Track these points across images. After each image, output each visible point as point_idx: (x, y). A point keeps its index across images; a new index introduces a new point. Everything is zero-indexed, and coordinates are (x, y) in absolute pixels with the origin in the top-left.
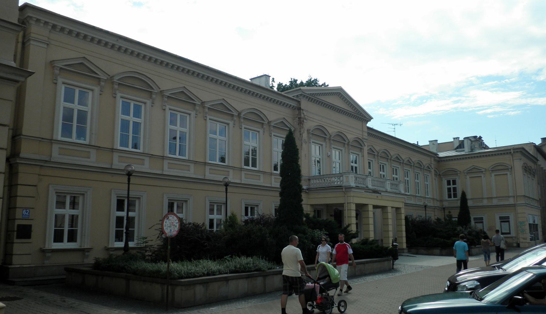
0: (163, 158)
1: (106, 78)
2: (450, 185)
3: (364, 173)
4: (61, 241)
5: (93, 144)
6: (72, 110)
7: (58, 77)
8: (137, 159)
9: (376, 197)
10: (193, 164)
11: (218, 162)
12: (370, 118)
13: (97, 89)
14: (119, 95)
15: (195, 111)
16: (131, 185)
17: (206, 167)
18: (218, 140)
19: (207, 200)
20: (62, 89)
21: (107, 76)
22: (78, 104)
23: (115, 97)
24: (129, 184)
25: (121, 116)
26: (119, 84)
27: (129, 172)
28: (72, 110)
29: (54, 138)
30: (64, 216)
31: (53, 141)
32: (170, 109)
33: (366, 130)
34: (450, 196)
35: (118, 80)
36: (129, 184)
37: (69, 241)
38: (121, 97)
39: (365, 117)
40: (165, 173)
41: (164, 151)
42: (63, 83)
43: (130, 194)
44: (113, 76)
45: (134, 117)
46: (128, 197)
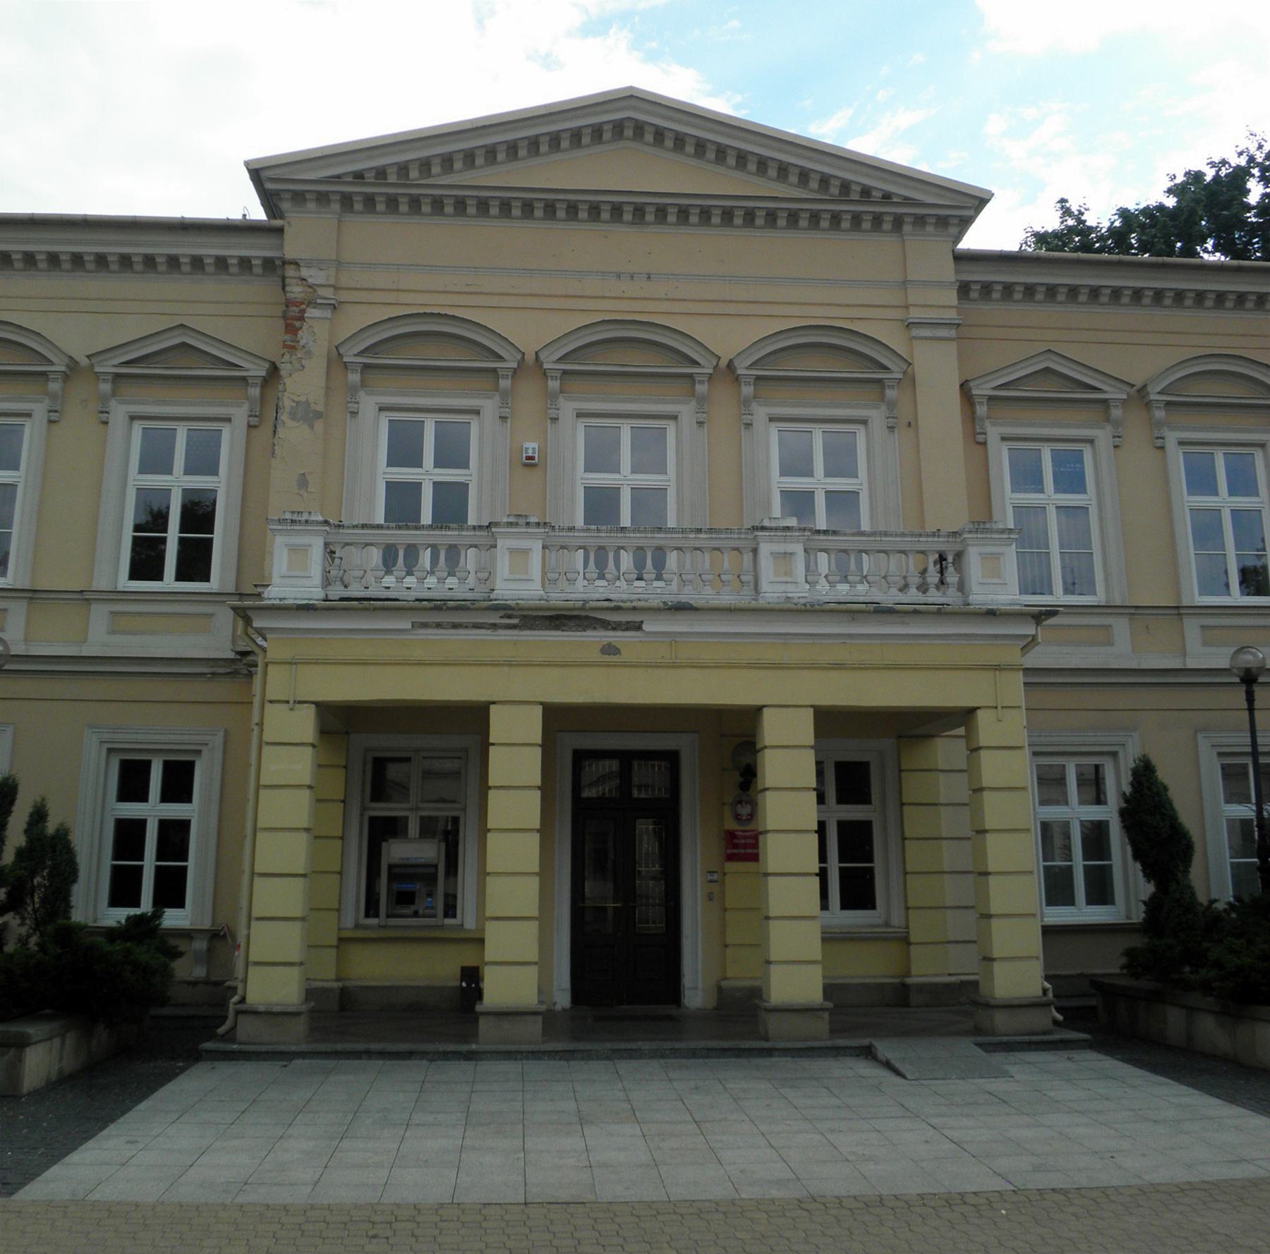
0: (1178, 611)
1: (1125, 397)
2: (415, 460)
3: (923, 527)
4: (1069, 901)
5: (1118, 603)
6: (416, 487)
7: (987, 424)
8: (1259, 627)
9: (596, 656)
10: (24, 604)
11: (1237, 597)
12: (970, 203)
13: (1103, 436)
14: (1172, 438)
15: (1109, 428)
16: (1257, 714)
17: (1186, 620)
18: (1052, 515)
19: (1204, 745)
20: (1177, 459)
21: (1128, 389)
22: (1230, 495)
23: (1162, 448)
24: (1251, 709)
25: (1188, 502)
26: (1168, 403)
27: (1248, 670)
28: (416, 487)
29: (1185, 603)
30: (1066, 826)
31: (1182, 611)
32: (1181, 443)
33: (948, 272)
34: (146, 563)
35: (752, 366)
36: (1251, 709)
37: (1090, 901)
38: (1003, 439)
39: (908, 202)
40: (1191, 664)
41: (1176, 582)
42: (772, 419)
43: (1259, 740)
44: (1145, 386)
45: (1231, 494)
46: (1255, 754)
